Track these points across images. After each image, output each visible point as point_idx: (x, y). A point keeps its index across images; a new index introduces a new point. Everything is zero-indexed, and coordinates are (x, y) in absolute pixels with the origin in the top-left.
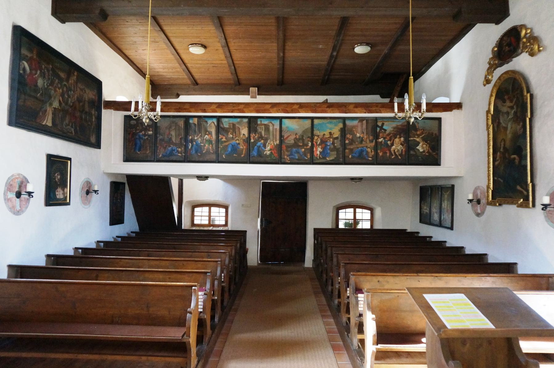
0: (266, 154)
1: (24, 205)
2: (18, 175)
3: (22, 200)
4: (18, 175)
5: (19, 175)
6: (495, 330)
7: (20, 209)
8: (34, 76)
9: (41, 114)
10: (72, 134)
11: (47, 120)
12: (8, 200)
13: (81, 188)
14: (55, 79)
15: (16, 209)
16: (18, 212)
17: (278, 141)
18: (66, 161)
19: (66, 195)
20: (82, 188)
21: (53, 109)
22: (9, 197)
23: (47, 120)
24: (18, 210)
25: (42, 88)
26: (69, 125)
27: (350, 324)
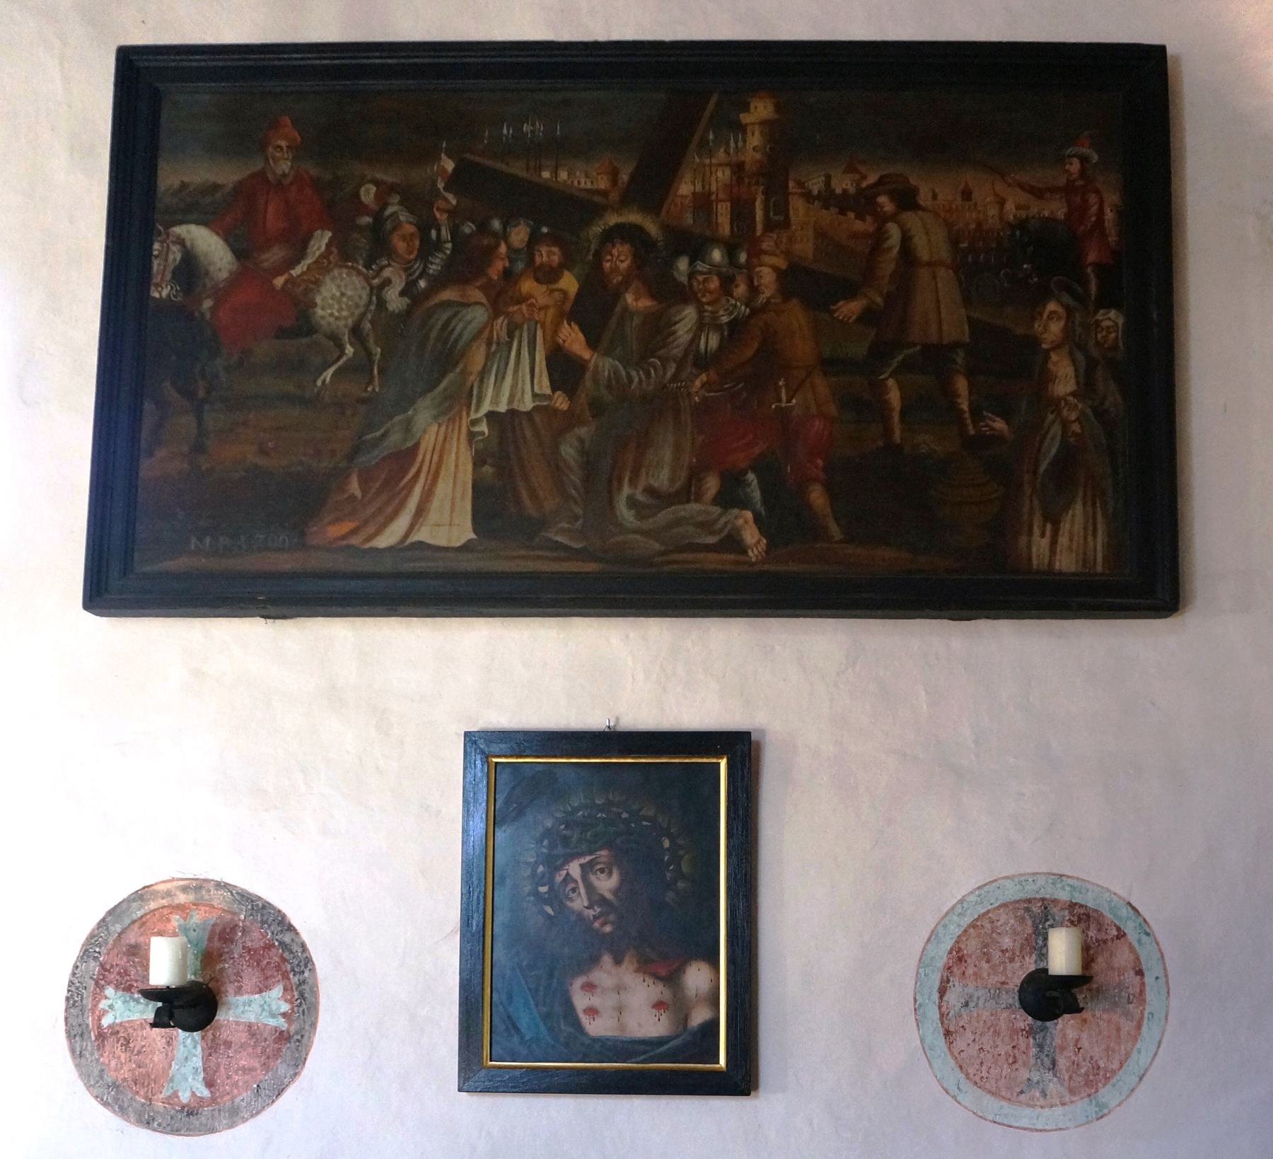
0: (1044, 215)
1: (246, 1070)
2: (185, 889)
3: (228, 1044)
4: (185, 889)
5: (198, 886)
6: (470, 564)
7: (204, 1092)
8: (279, 281)
9: (354, 486)
10: (741, 548)
11: (420, 512)
12: (101, 1036)
13: (941, 953)
14: (496, 224)
15: (166, 1092)
16: (190, 1111)
17: (155, 268)
18: (715, 761)
19: (699, 1017)
20: (958, 957)
21: (483, 428)
22: (106, 1021)
23: (420, 512)
24: (185, 1097)
25: (356, 331)
26: (688, 492)
27: (1149, 926)
